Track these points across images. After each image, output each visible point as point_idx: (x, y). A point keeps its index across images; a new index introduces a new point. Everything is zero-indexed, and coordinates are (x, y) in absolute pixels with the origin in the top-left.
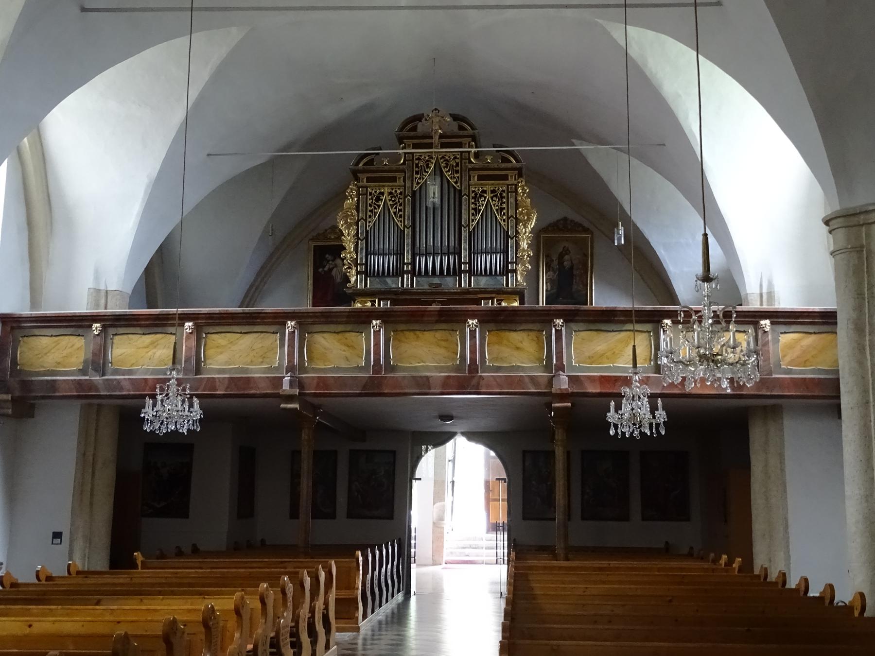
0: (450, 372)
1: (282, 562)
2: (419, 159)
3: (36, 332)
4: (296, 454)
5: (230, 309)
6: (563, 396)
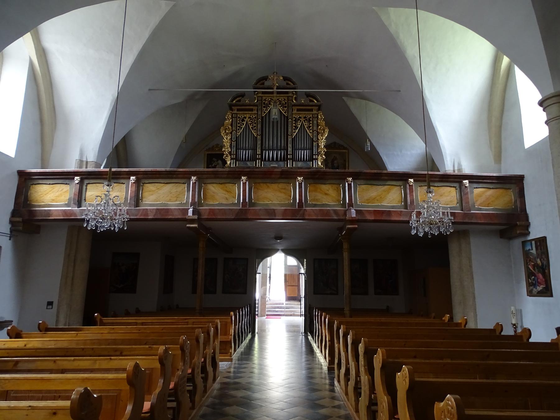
0: (288, 207)
1: (186, 319)
2: (265, 100)
3: (40, 182)
4: (196, 260)
5: (158, 169)
6: (353, 221)
